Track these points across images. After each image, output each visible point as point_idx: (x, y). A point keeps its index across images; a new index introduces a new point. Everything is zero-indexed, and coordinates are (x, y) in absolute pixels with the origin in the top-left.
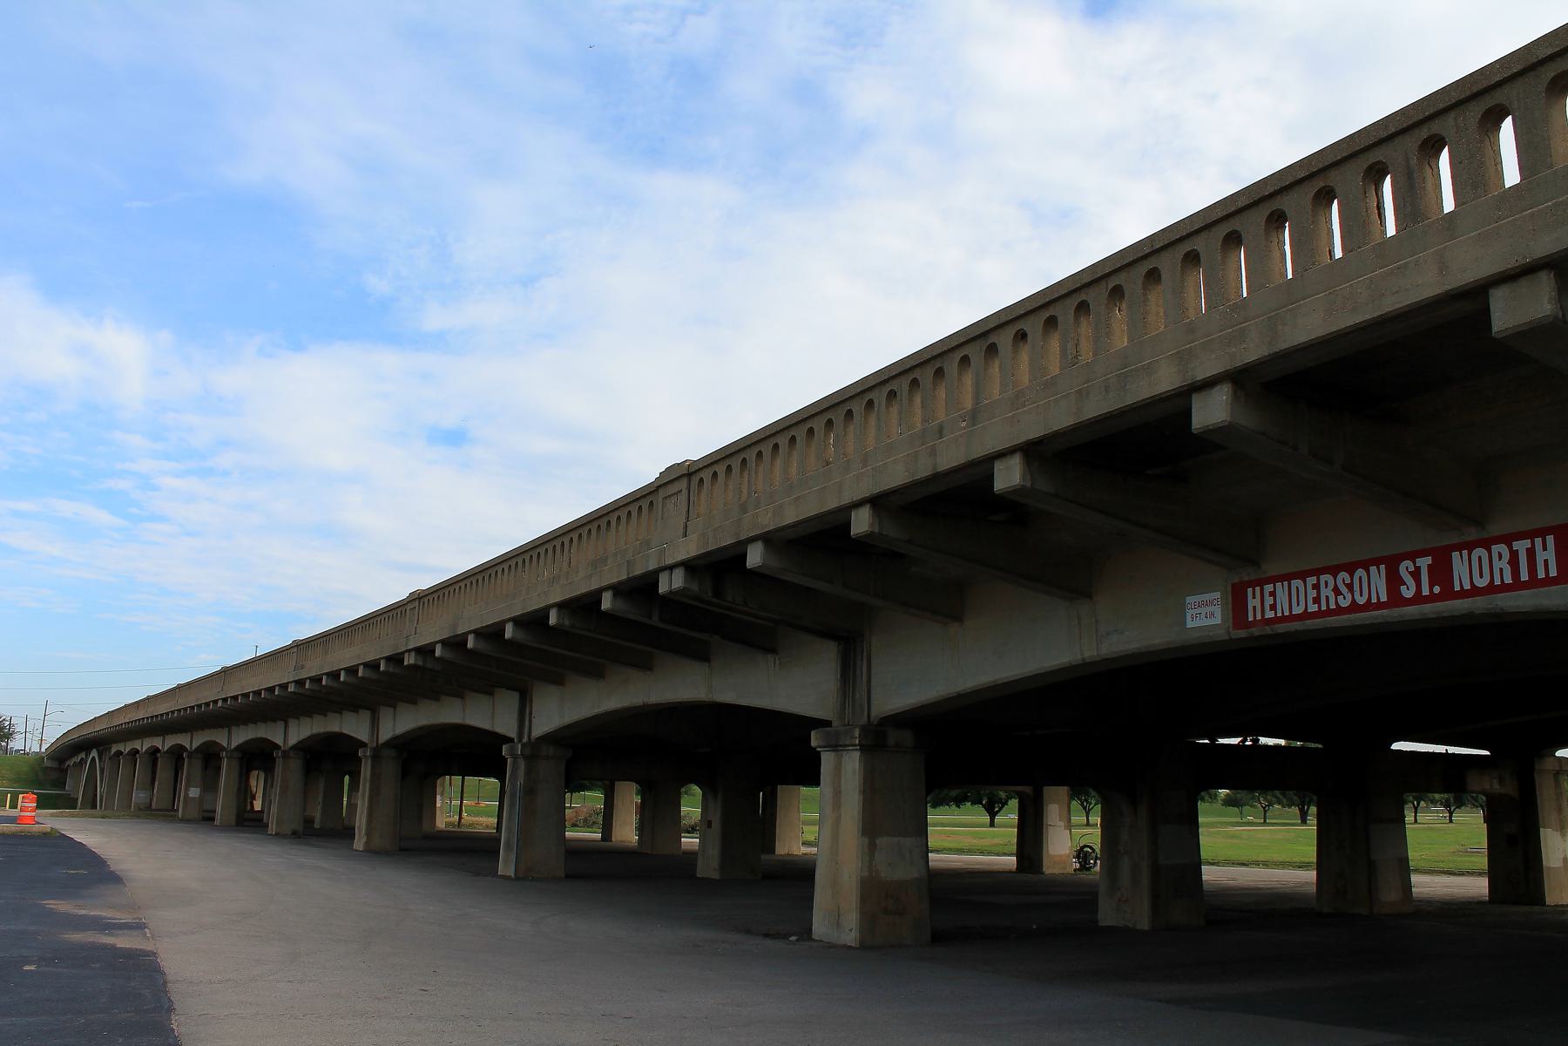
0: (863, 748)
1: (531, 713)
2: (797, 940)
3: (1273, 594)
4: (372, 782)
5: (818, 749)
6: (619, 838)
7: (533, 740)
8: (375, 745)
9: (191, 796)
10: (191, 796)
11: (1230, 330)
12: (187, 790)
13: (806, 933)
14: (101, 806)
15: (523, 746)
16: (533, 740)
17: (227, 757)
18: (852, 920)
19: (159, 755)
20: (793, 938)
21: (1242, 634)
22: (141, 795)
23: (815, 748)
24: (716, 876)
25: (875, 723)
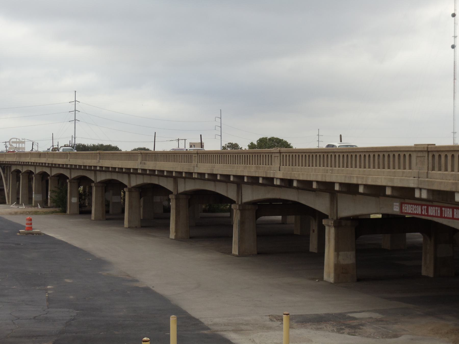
0: (335, 227)
1: (241, 193)
2: (318, 281)
3: (406, 207)
4: (176, 209)
5: (325, 225)
6: (456, 143)
7: (243, 203)
8: (176, 193)
9: (73, 202)
10: (73, 202)
11: (342, 175)
12: (70, 199)
13: (322, 278)
14: (9, 202)
15: (239, 206)
16: (243, 203)
17: (95, 186)
18: (332, 275)
19: (49, 178)
20: (317, 280)
21: (402, 214)
22: (38, 197)
23: (324, 225)
24: (316, 251)
25: (339, 219)
